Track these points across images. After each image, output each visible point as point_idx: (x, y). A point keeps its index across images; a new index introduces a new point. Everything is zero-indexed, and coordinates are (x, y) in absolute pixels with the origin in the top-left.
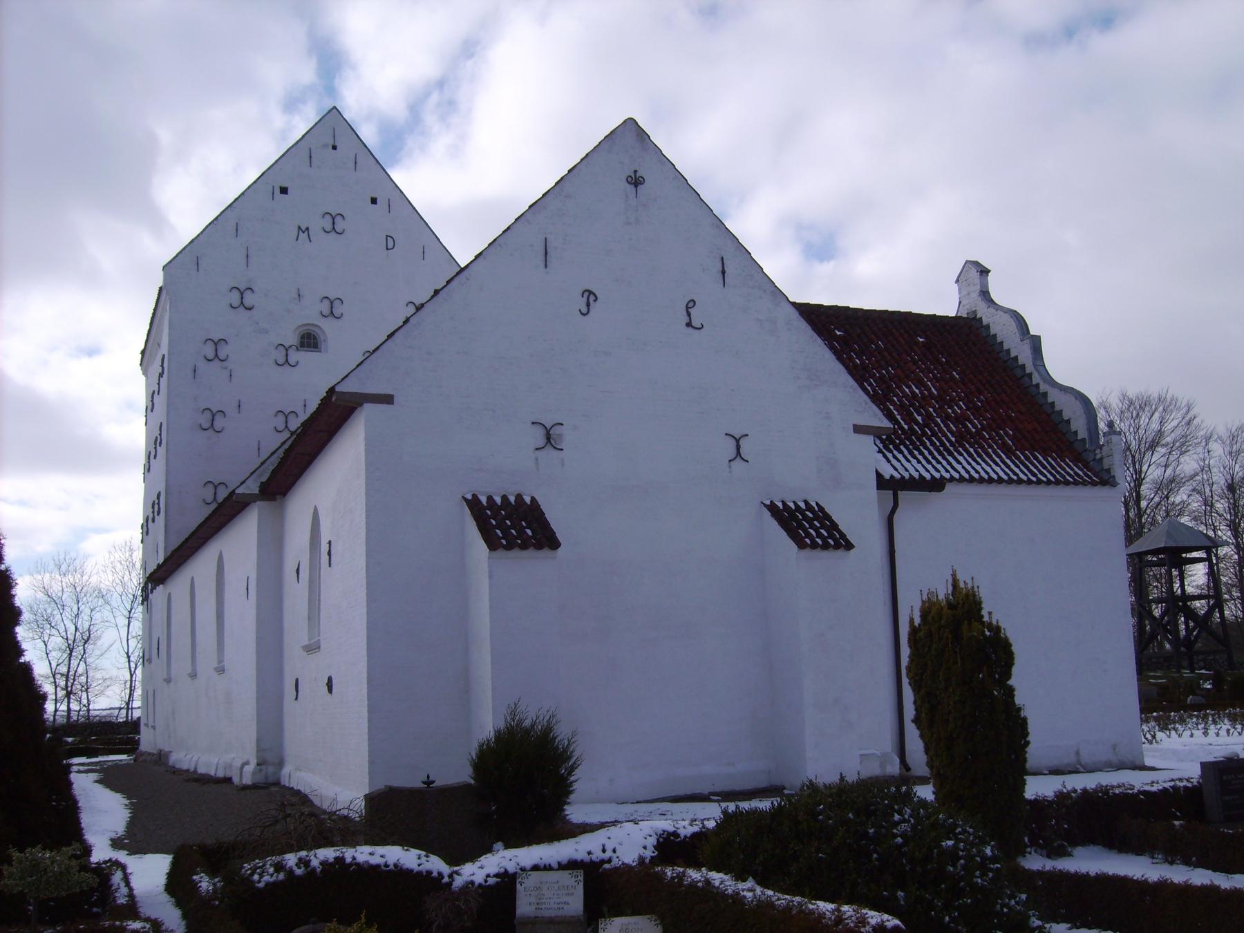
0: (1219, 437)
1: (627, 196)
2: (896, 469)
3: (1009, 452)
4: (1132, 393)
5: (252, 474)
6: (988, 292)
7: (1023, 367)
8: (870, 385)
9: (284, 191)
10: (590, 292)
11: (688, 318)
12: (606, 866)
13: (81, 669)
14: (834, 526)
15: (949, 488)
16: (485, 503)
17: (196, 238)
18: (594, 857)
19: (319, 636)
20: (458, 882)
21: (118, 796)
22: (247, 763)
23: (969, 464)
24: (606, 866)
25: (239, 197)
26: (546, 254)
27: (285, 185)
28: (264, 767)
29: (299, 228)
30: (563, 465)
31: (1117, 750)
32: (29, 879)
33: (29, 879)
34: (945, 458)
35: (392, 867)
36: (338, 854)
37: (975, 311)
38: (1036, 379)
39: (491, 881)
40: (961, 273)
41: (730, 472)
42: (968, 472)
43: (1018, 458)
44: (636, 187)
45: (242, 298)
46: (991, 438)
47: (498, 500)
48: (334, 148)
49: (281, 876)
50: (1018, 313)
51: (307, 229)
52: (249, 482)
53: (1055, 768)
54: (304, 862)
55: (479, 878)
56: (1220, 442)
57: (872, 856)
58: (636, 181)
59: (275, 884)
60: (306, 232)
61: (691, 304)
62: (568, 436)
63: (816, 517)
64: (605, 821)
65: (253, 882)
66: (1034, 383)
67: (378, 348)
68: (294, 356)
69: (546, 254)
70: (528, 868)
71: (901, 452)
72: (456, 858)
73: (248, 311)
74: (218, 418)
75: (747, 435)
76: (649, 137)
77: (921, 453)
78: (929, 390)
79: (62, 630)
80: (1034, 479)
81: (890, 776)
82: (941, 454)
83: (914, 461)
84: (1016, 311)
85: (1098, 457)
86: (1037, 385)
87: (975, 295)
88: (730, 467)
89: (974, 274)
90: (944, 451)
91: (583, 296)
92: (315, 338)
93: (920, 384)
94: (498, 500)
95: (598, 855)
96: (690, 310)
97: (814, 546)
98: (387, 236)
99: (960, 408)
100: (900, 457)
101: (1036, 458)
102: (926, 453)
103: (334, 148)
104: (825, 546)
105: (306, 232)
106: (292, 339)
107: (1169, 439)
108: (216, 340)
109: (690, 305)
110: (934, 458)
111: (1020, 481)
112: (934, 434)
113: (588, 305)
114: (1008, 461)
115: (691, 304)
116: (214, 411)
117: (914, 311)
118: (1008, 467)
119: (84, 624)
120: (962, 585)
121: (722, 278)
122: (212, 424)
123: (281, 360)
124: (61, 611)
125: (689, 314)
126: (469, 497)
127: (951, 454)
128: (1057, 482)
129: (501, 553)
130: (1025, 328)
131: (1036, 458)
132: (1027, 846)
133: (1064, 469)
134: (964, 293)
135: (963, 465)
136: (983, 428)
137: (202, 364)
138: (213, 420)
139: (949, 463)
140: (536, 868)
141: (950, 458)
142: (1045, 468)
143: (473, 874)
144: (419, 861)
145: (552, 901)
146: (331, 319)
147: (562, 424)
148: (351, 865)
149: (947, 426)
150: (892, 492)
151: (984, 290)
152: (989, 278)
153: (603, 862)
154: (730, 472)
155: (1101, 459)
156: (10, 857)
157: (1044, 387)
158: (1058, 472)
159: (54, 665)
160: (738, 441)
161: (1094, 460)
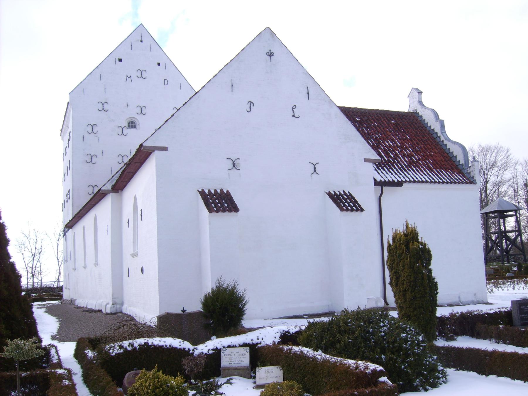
0: (520, 163)
2: (382, 177)
3: (430, 169)
4: (483, 145)
5: (108, 181)
6: (422, 101)
7: (437, 133)
8: (371, 141)
9: (120, 60)
10: (251, 102)
12: (259, 345)
13: (38, 265)
14: (356, 202)
15: (405, 184)
20: (197, 353)
23: (414, 175)
24: (259, 345)
25: (101, 63)
26: (232, 86)
27: (120, 58)
29: (127, 76)
30: (240, 176)
31: (476, 296)
34: (403, 173)
35: (168, 346)
36: (146, 341)
38: (442, 138)
39: (211, 352)
40: (410, 93)
42: (413, 178)
43: (434, 172)
44: (270, 57)
45: (103, 107)
46: (423, 164)
47: (213, 192)
48: (141, 41)
49: (122, 351)
50: (435, 111)
51: (131, 76)
53: (450, 304)
55: (205, 351)
56: (520, 165)
58: (270, 55)
59: (119, 354)
60: (130, 78)
61: (294, 107)
62: (241, 164)
63: (348, 198)
66: (441, 140)
68: (126, 131)
69: (232, 86)
71: (384, 170)
72: (195, 343)
74: (94, 158)
75: (319, 163)
76: (276, 35)
77: (393, 170)
78: (396, 143)
80: (441, 181)
82: (401, 170)
83: (390, 174)
84: (433, 110)
86: (443, 141)
88: (311, 177)
89: (416, 94)
90: (403, 169)
91: (248, 104)
92: (134, 123)
93: (392, 141)
94: (213, 192)
96: (294, 110)
97: (347, 210)
98: (165, 79)
99: (410, 151)
100: (384, 172)
101: (442, 172)
102: (395, 170)
103: (141, 41)
104: (352, 210)
105: (130, 78)
106: (126, 124)
107: (499, 164)
110: (398, 172)
111: (435, 182)
112: (399, 162)
113: (250, 108)
114: (430, 174)
115: (294, 107)
117: (390, 110)
118: (430, 176)
120: (410, 226)
122: (91, 161)
123: (120, 133)
125: (293, 112)
126: (200, 190)
127: (405, 171)
128: (451, 183)
129: (214, 214)
130: (437, 115)
131: (442, 172)
132: (437, 336)
133: (454, 177)
134: (411, 102)
135: (411, 175)
136: (419, 160)
137: (87, 136)
138: (91, 159)
139: (405, 175)
140: (229, 346)
141: (405, 172)
142: (446, 176)
144: (180, 344)
145: (236, 360)
146: (141, 115)
147: (240, 159)
148: (151, 346)
149: (404, 159)
150: (380, 187)
153: (258, 344)
155: (470, 172)
157: (445, 142)
159: (26, 264)
160: (315, 166)
161: (467, 173)
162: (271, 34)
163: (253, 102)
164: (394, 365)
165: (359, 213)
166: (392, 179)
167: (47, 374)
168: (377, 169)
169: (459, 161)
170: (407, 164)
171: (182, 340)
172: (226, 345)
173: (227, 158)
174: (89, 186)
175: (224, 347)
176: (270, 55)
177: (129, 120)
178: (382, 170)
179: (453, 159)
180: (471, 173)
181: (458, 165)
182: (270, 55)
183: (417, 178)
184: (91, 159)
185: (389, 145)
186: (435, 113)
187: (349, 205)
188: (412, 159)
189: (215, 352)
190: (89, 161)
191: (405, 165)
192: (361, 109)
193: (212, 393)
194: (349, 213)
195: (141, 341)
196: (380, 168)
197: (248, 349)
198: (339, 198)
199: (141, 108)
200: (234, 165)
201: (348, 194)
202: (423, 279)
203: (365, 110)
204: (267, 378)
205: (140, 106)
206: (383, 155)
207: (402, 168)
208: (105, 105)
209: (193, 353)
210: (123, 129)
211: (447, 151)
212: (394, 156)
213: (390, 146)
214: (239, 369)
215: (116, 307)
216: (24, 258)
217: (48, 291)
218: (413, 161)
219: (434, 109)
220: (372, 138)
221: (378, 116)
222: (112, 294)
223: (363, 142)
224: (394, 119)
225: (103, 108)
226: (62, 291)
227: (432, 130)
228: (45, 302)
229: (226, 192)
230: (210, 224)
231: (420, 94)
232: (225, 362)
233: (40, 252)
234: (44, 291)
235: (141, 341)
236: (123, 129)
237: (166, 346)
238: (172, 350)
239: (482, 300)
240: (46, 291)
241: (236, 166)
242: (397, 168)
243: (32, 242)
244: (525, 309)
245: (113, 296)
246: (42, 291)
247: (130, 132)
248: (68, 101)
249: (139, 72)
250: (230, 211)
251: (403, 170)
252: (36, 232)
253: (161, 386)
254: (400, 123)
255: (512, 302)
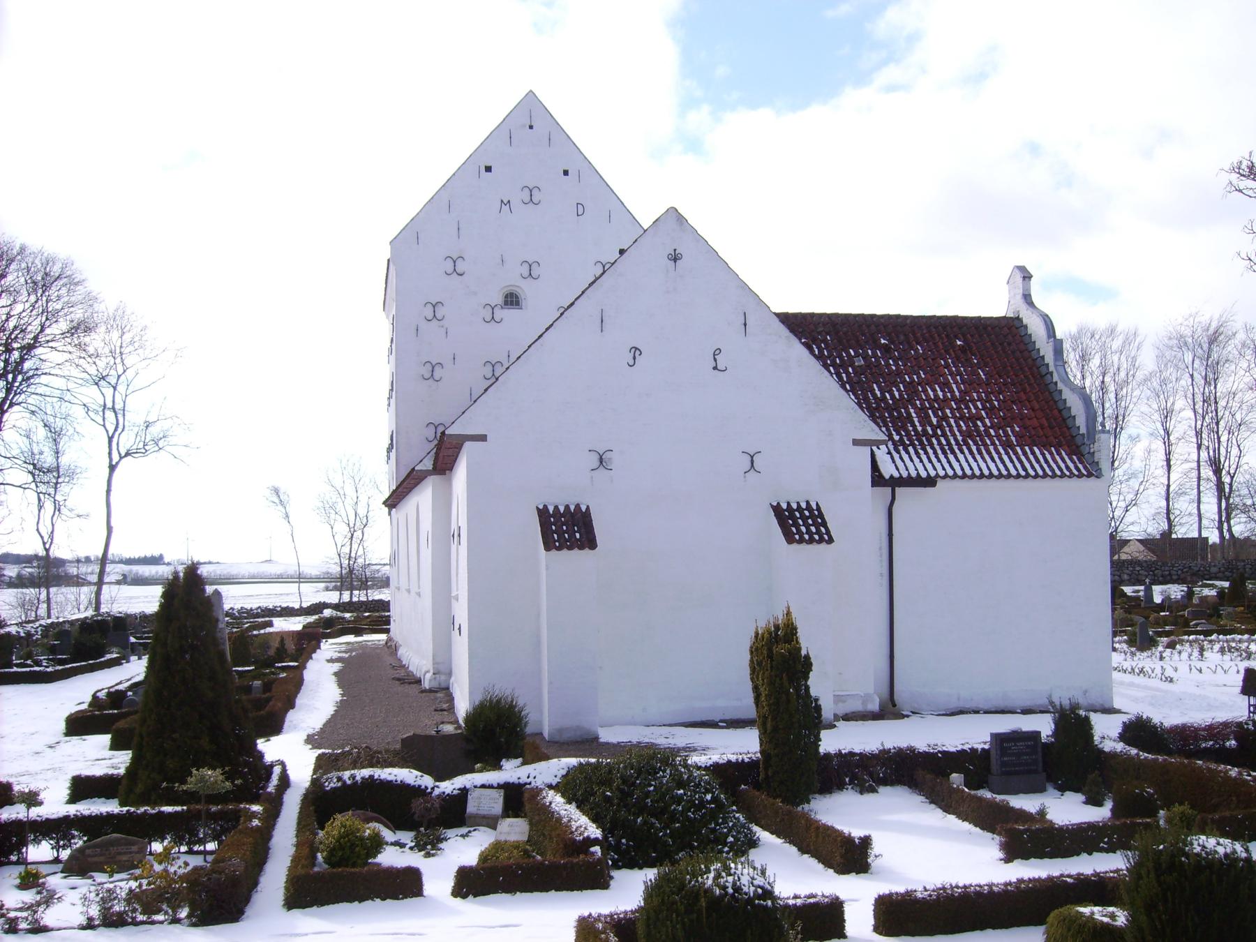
1: (667, 271)
2: (897, 469)
3: (1007, 445)
5: (428, 454)
6: (1030, 295)
8: (899, 390)
10: (636, 349)
11: (715, 363)
12: (528, 786)
13: (360, 552)
14: (824, 524)
15: (940, 483)
16: (551, 512)
17: (416, 216)
18: (521, 781)
19: (457, 590)
20: (437, 792)
21: (339, 691)
22: (428, 672)
24: (528, 786)
25: (451, 178)
26: (602, 321)
27: (488, 165)
28: (437, 676)
29: (502, 201)
30: (612, 481)
31: (1087, 694)
32: (199, 785)
33: (199, 785)
35: (399, 782)
36: (372, 773)
37: (1019, 311)
39: (456, 792)
40: (1010, 276)
41: (745, 481)
43: (1016, 454)
44: (675, 262)
46: (998, 436)
47: (562, 509)
48: (531, 127)
49: (340, 784)
50: (1049, 318)
51: (509, 202)
52: (425, 461)
53: (1028, 708)
54: (353, 777)
55: (448, 791)
57: (741, 786)
59: (335, 788)
60: (508, 205)
61: (717, 352)
62: (616, 459)
64: (622, 741)
65: (325, 787)
66: (1054, 381)
67: (572, 304)
68: (499, 314)
69: (602, 321)
70: (478, 786)
71: (908, 452)
72: (440, 778)
73: (460, 277)
74: (437, 369)
76: (687, 221)
77: (926, 453)
78: (952, 392)
79: (344, 515)
81: (870, 712)
84: (1047, 316)
85: (1092, 450)
86: (1056, 383)
87: (1019, 298)
88: (745, 477)
90: (947, 450)
92: (517, 297)
94: (562, 509)
95: (524, 780)
96: (716, 357)
97: (801, 541)
99: (976, 408)
100: (905, 457)
103: (531, 127)
105: (508, 205)
106: (498, 299)
108: (434, 303)
109: (717, 353)
110: (937, 457)
112: (944, 435)
113: (634, 358)
115: (717, 352)
116: (434, 364)
119: (362, 512)
121: (744, 329)
122: (432, 375)
123: (488, 318)
124: (343, 499)
125: (715, 360)
126: (541, 507)
127: (953, 452)
129: (554, 553)
131: (1033, 453)
133: (1056, 462)
135: (963, 461)
137: (424, 326)
138: (433, 371)
139: (949, 462)
140: (483, 786)
143: (446, 788)
144: (415, 779)
145: (486, 806)
146: (530, 280)
148: (377, 780)
151: (1027, 293)
152: (1031, 282)
153: (526, 784)
154: (745, 481)
155: (1094, 453)
156: (192, 773)
157: (1060, 386)
158: (1049, 466)
159: (339, 547)
160: (752, 457)
161: (1089, 453)
162: (678, 219)
163: (640, 348)
164: (649, 831)
165: (823, 545)
166: (918, 473)
167: (240, 810)
168: (893, 452)
169: (1079, 427)
170: (960, 438)
171: (420, 774)
172: (479, 783)
173: (590, 451)
174: (428, 425)
175: (475, 787)
176: (675, 258)
177: (506, 291)
178: (903, 452)
179: (1069, 422)
180: (1096, 454)
181: (1076, 436)
182: (675, 258)
183: (971, 469)
184: (433, 371)
185: (936, 395)
186: (1046, 318)
187: (809, 531)
188: (976, 426)
189: (462, 792)
190: (427, 375)
191: (956, 440)
192: (898, 316)
193: (428, 847)
194: (804, 546)
195: (366, 772)
196: (901, 448)
197: (502, 792)
198: (792, 516)
199: (530, 266)
200: (601, 462)
201: (815, 507)
202: (788, 701)
203: (906, 317)
204: (509, 833)
205: (526, 262)
206: (916, 420)
207: (946, 448)
208: (459, 262)
209: (431, 793)
210: (493, 309)
211: (1061, 406)
212: (938, 422)
213: (937, 398)
214: (488, 818)
215: (438, 678)
216: (334, 534)
217: (377, 608)
218: (977, 430)
219: (1049, 315)
220: (904, 382)
221: (929, 332)
222: (433, 656)
223: (853, 409)
224: (964, 335)
225: (455, 270)
226: (389, 624)
227: (1041, 357)
228: (362, 636)
229: (584, 511)
230: (547, 569)
231: (1027, 279)
232: (471, 808)
233: (364, 523)
234: (368, 607)
235: (366, 772)
236: (493, 309)
237: (396, 781)
238: (404, 788)
239: (1101, 702)
240: (371, 609)
241: (604, 464)
242: (937, 448)
243: (349, 502)
244: (1013, 748)
245: (433, 659)
246: (364, 607)
247: (509, 314)
248: (389, 256)
249: (527, 190)
250: (581, 548)
251: (948, 452)
252: (357, 482)
253: (347, 835)
254: (973, 345)
255: (992, 735)
